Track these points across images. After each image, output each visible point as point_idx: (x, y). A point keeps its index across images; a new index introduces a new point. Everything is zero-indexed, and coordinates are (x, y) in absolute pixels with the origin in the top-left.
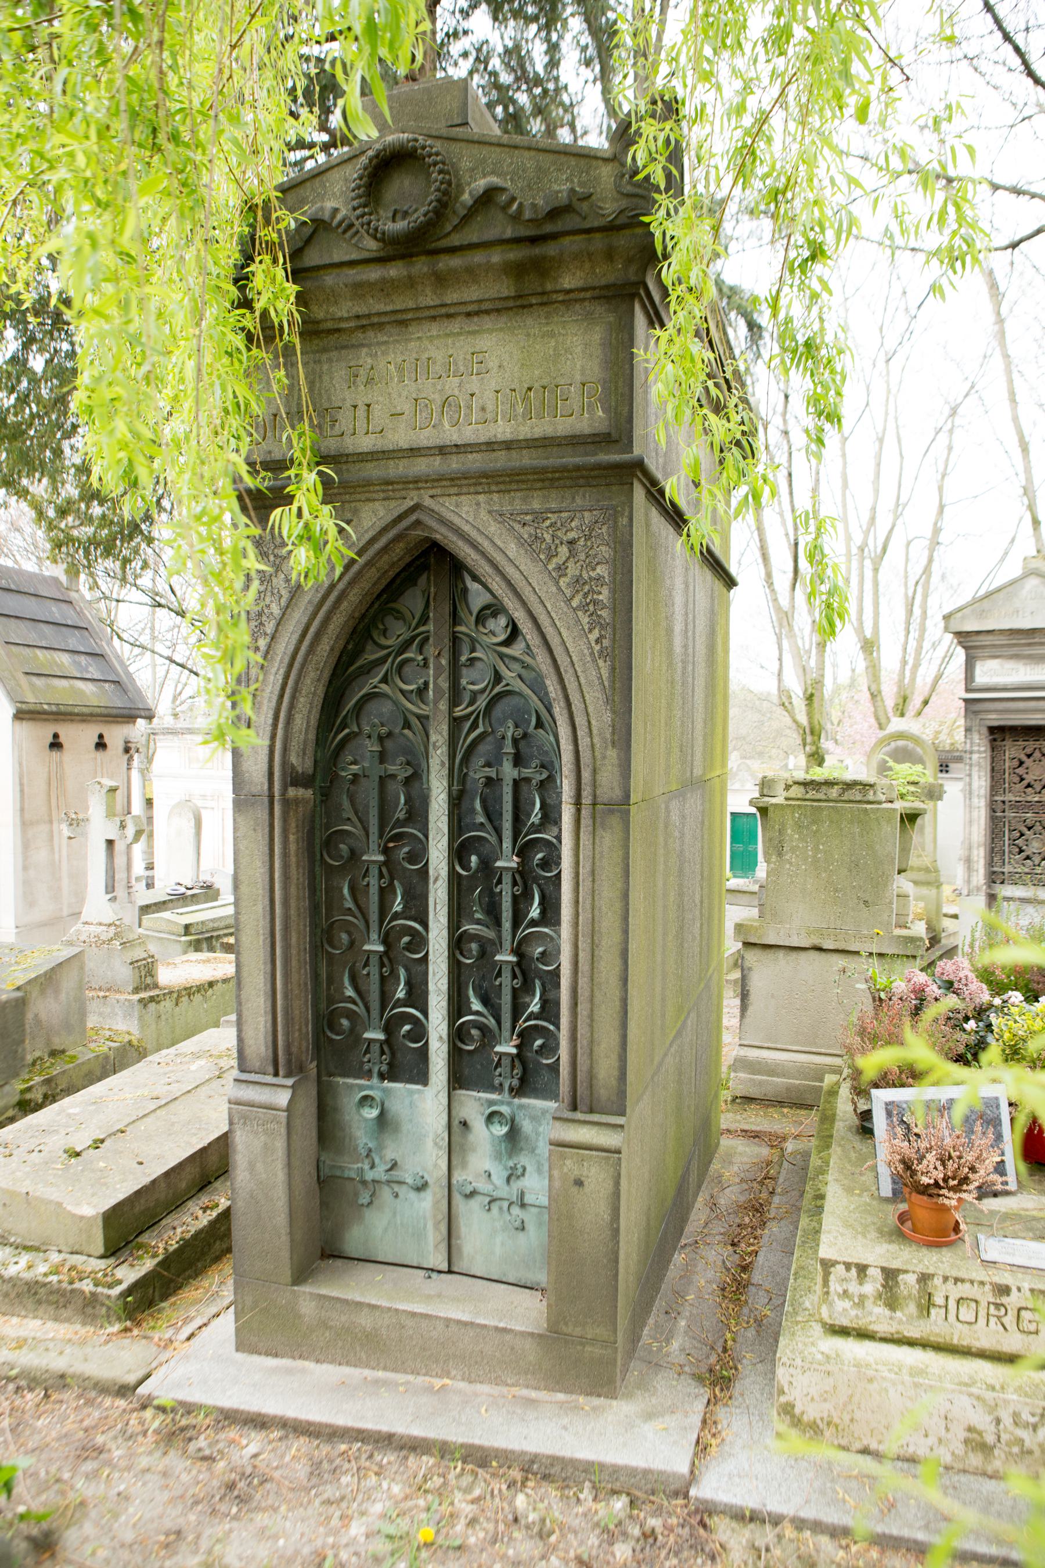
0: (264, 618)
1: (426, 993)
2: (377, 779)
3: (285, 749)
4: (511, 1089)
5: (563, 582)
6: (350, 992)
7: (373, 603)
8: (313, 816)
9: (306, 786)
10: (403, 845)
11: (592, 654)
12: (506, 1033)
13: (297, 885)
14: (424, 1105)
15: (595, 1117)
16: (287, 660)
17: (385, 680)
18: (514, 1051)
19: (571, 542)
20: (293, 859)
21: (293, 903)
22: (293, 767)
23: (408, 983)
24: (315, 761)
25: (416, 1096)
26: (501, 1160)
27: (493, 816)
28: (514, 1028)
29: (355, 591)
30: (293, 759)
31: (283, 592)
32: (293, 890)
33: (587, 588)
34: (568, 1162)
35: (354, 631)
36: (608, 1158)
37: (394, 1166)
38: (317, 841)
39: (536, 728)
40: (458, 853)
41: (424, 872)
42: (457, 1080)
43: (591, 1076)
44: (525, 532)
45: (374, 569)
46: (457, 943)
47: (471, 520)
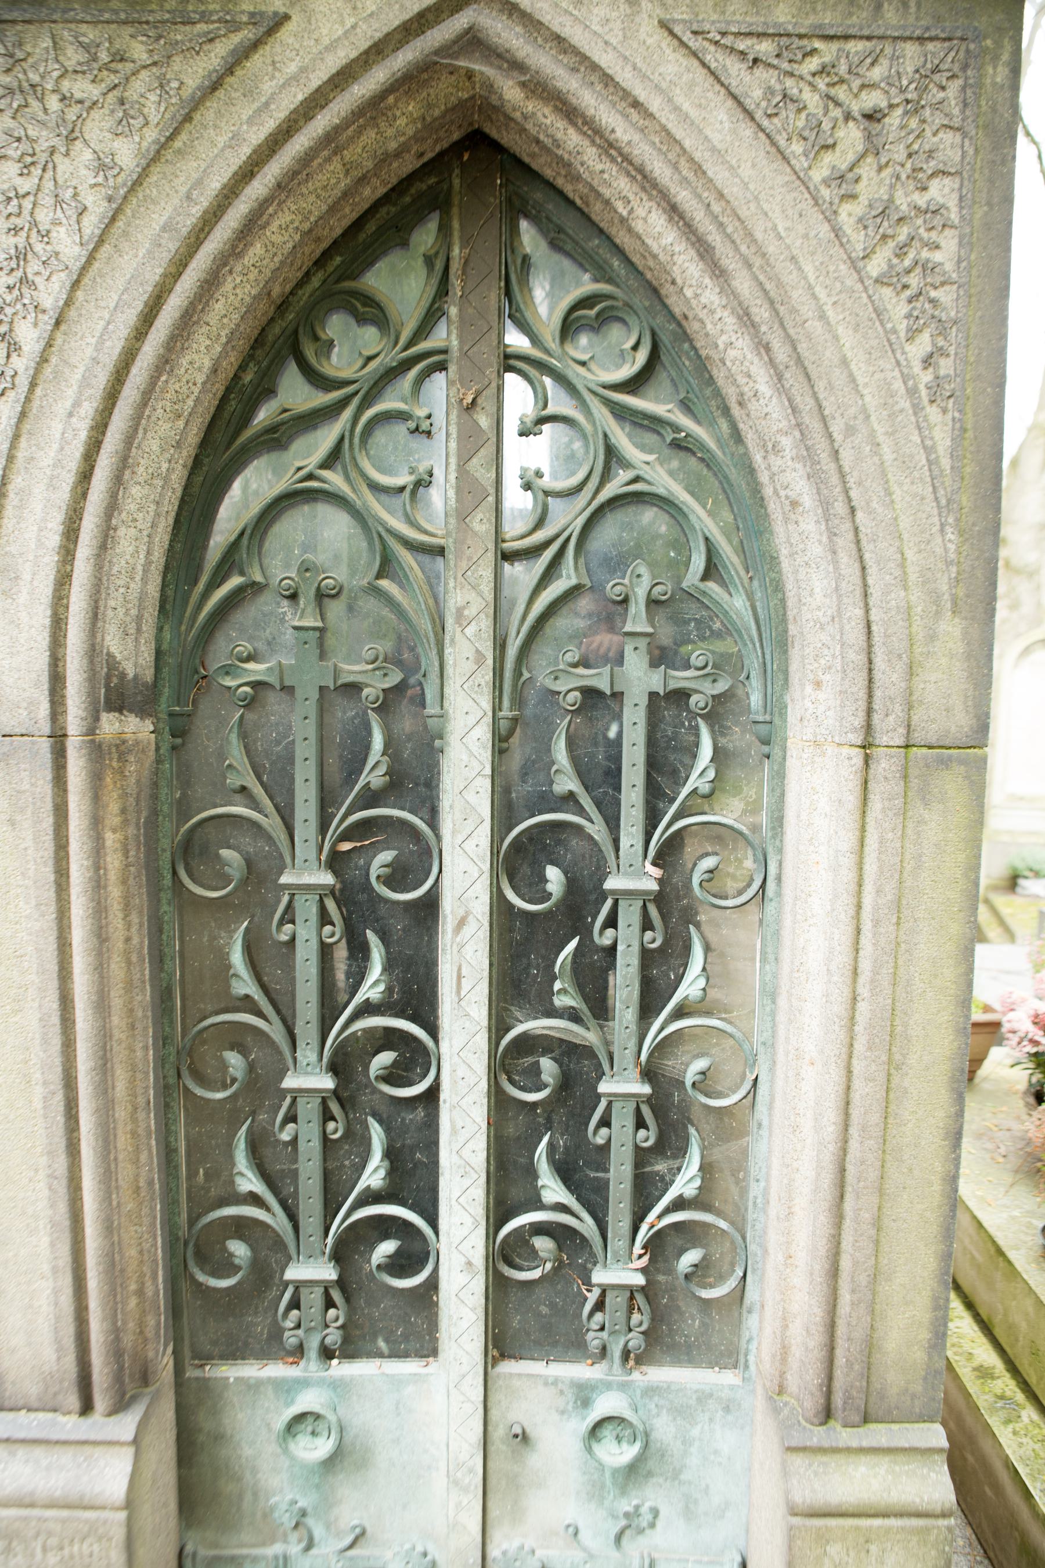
0: (33, 266)
1: (433, 1167)
2: (315, 695)
3: (95, 616)
4: (626, 1355)
5: (848, 214)
6: (249, 1182)
7: (308, 275)
8: (155, 785)
9: (142, 713)
10: (376, 848)
11: (912, 392)
12: (617, 1243)
13: (127, 953)
14: (423, 1404)
15: (878, 1434)
16: (102, 379)
17: (332, 459)
18: (640, 1280)
19: (872, 117)
20: (115, 892)
21: (117, 1001)
22: (112, 663)
23: (389, 1154)
24: (159, 654)
25: (410, 1389)
26: (602, 1499)
27: (603, 778)
28: (635, 1230)
29: (285, 218)
30: (113, 643)
31: (89, 198)
32: (116, 968)
33: (903, 233)
34: (834, 1550)
35: (258, 342)
36: (927, 1530)
37: (360, 1537)
38: (165, 843)
39: (706, 576)
40: (517, 860)
41: (428, 909)
42: (500, 1344)
43: (870, 1346)
44: (754, 85)
45: (336, 165)
46: (510, 1060)
47: (614, 41)
